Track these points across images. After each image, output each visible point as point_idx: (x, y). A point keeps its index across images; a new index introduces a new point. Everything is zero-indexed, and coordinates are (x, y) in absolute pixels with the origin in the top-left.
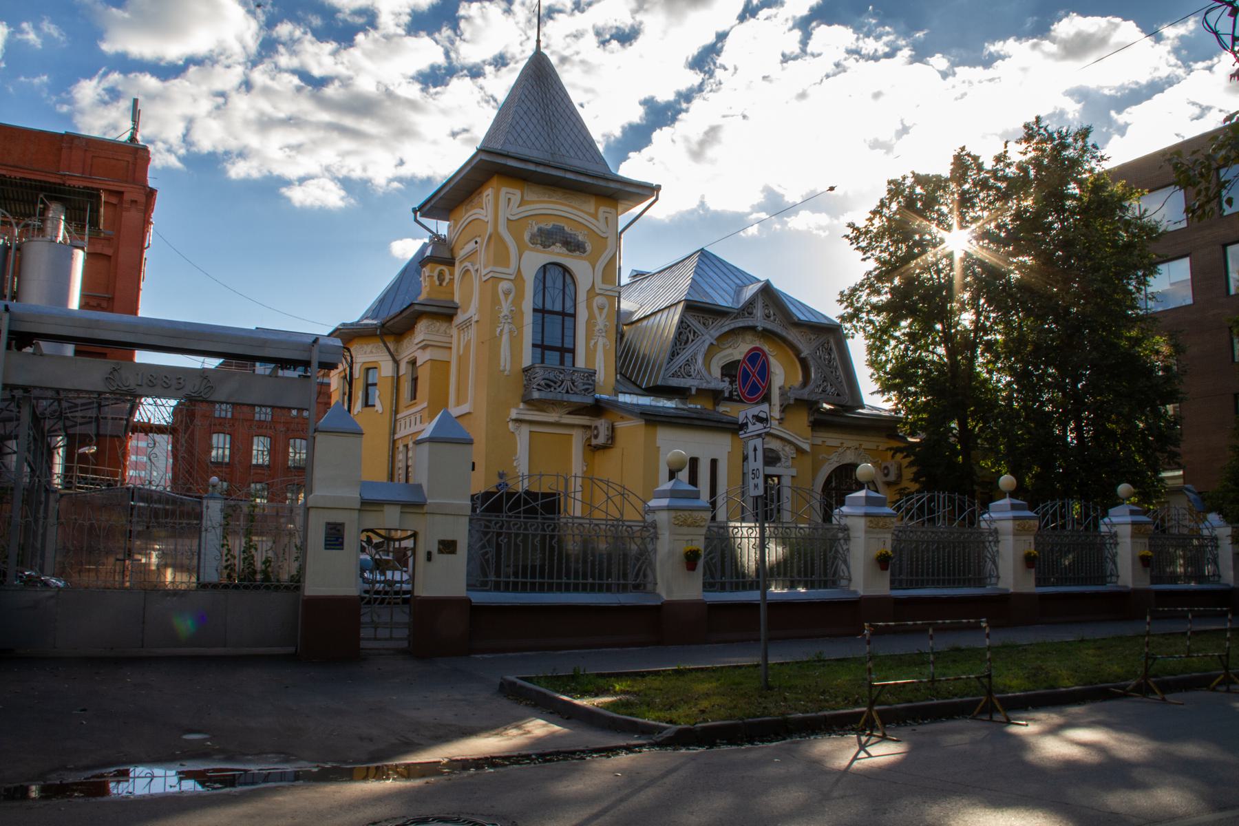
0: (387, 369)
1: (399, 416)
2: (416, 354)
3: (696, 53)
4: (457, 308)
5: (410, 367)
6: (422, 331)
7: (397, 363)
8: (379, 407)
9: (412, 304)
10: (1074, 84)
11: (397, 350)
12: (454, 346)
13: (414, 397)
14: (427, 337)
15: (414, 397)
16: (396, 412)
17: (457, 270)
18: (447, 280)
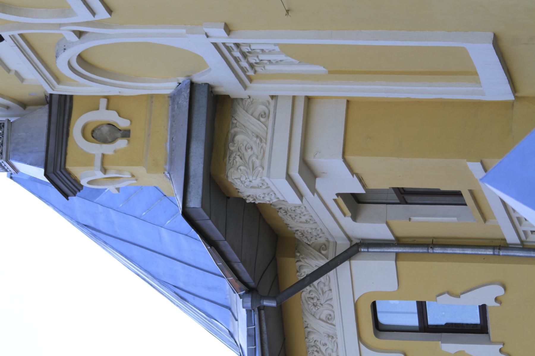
0: (373, 275)
1: (512, 238)
2: (330, 197)
3: (506, 78)
4: (192, 85)
5: (369, 209)
6: (261, 177)
7: (356, 248)
8: (487, 295)
9: (186, 215)
10: (87, 181)
11: (321, 248)
12: (302, 89)
13: (454, 197)
14: (279, 168)
15: (454, 197)
16: (501, 245)
17: (79, 87)
18: (112, 117)
